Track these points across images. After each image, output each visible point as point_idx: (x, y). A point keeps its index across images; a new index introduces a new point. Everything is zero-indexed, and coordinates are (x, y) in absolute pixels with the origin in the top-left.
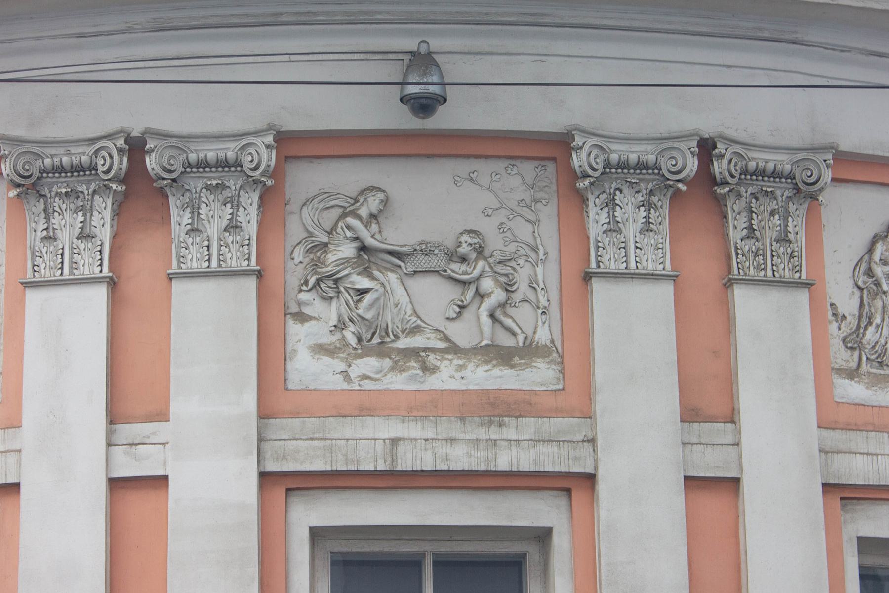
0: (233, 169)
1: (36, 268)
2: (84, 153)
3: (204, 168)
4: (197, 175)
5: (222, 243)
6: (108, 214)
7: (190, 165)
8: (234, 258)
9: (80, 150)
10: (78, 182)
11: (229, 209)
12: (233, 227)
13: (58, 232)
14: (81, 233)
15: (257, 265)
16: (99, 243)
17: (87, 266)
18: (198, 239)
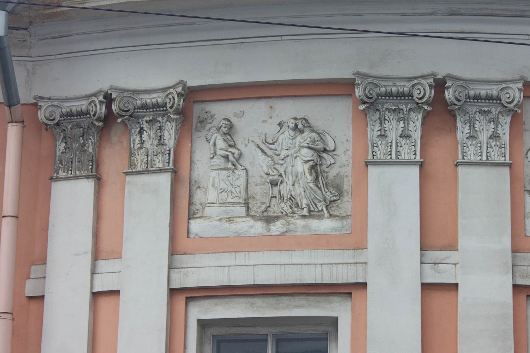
0: (495, 101)
1: (374, 153)
2: (405, 86)
3: (478, 100)
4: (473, 104)
5: (488, 145)
6: (419, 124)
7: (469, 98)
8: (496, 155)
9: (402, 84)
10: (400, 103)
11: (492, 126)
12: (495, 136)
13: (388, 132)
14: (402, 134)
15: (421, 158)
16: (414, 141)
17: (406, 154)
18: (474, 142)
